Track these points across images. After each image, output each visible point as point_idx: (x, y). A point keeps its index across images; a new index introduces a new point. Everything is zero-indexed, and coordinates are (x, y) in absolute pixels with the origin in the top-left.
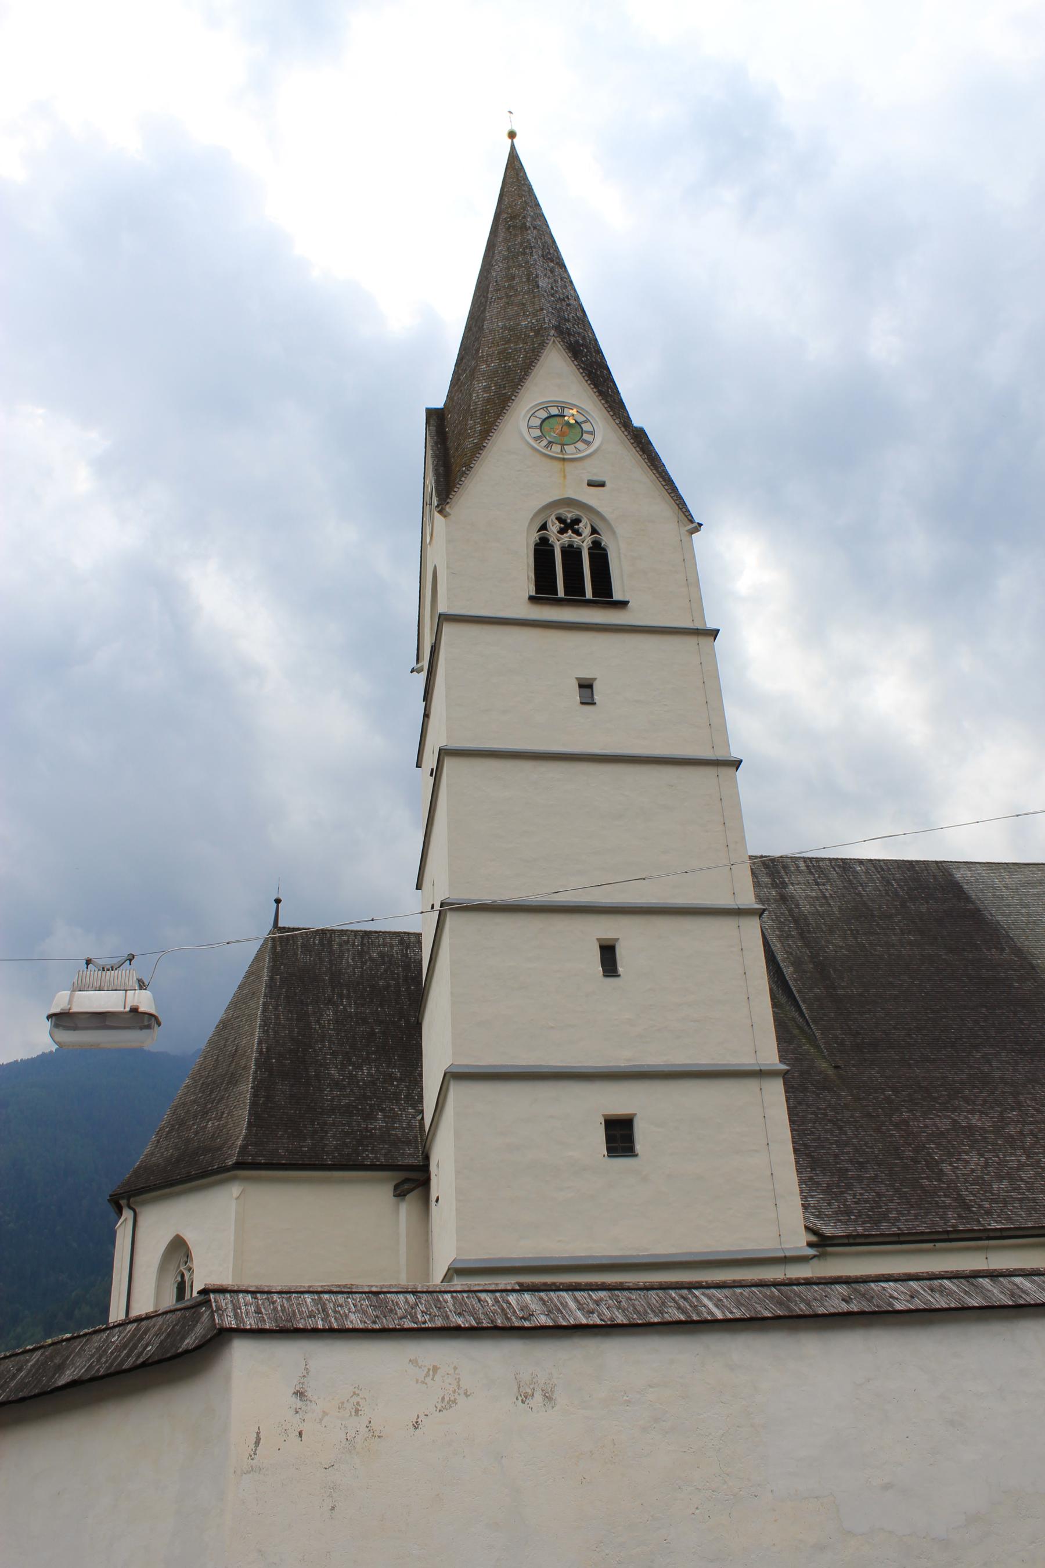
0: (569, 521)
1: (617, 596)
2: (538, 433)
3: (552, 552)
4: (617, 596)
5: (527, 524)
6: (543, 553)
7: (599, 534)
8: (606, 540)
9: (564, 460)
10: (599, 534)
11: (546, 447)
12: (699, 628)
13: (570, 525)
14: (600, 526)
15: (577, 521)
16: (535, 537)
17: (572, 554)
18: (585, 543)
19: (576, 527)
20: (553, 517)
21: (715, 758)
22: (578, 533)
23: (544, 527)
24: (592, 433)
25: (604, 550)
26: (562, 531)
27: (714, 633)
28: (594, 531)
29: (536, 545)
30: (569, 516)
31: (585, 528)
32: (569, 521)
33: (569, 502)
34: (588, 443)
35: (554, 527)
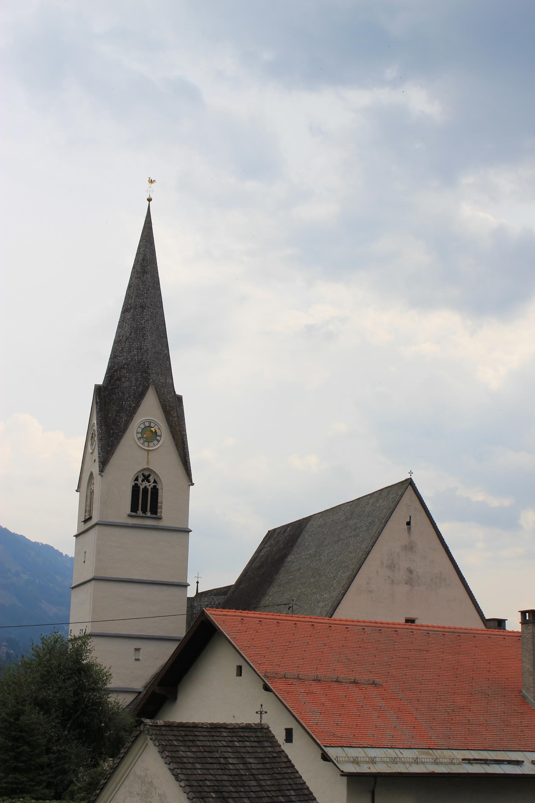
0: (146, 476)
1: (520, 613)
2: (139, 435)
3: (139, 491)
4: (520, 613)
5: (133, 476)
6: (135, 489)
7: (157, 483)
8: (158, 487)
9: (148, 450)
10: (157, 483)
11: (143, 444)
12: (514, 630)
13: (146, 478)
14: (157, 480)
15: (149, 475)
16: (133, 483)
17: (145, 490)
18: (150, 486)
19: (145, 480)
20: (141, 474)
21: (516, 760)
22: (149, 481)
23: (137, 479)
24: (160, 436)
25: (158, 489)
26: (143, 481)
27: (188, 531)
28: (155, 482)
29: (133, 487)
30: (147, 473)
31: (151, 479)
32: (146, 476)
33: (148, 469)
34: (158, 441)
35: (140, 480)
